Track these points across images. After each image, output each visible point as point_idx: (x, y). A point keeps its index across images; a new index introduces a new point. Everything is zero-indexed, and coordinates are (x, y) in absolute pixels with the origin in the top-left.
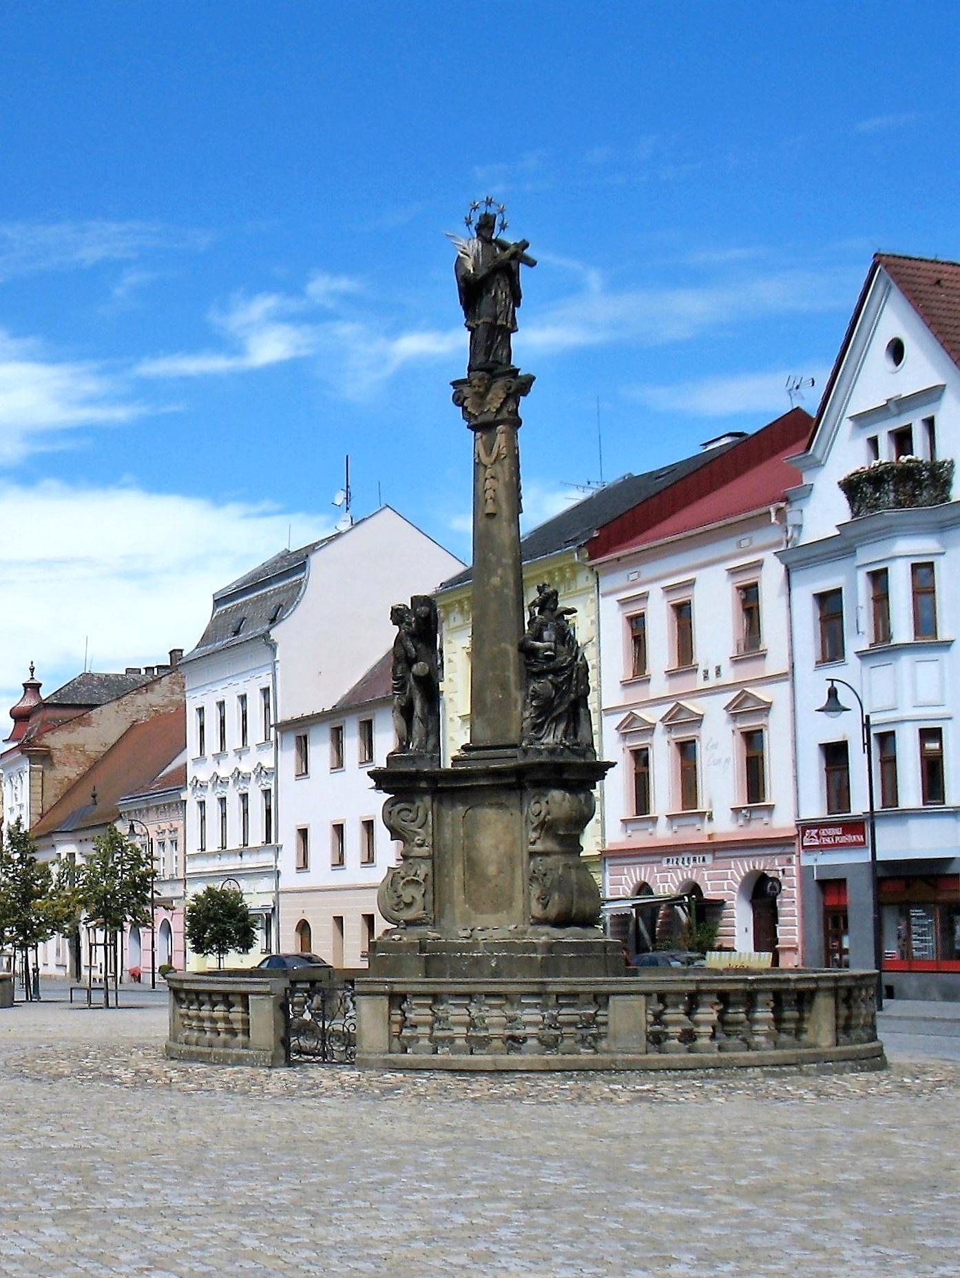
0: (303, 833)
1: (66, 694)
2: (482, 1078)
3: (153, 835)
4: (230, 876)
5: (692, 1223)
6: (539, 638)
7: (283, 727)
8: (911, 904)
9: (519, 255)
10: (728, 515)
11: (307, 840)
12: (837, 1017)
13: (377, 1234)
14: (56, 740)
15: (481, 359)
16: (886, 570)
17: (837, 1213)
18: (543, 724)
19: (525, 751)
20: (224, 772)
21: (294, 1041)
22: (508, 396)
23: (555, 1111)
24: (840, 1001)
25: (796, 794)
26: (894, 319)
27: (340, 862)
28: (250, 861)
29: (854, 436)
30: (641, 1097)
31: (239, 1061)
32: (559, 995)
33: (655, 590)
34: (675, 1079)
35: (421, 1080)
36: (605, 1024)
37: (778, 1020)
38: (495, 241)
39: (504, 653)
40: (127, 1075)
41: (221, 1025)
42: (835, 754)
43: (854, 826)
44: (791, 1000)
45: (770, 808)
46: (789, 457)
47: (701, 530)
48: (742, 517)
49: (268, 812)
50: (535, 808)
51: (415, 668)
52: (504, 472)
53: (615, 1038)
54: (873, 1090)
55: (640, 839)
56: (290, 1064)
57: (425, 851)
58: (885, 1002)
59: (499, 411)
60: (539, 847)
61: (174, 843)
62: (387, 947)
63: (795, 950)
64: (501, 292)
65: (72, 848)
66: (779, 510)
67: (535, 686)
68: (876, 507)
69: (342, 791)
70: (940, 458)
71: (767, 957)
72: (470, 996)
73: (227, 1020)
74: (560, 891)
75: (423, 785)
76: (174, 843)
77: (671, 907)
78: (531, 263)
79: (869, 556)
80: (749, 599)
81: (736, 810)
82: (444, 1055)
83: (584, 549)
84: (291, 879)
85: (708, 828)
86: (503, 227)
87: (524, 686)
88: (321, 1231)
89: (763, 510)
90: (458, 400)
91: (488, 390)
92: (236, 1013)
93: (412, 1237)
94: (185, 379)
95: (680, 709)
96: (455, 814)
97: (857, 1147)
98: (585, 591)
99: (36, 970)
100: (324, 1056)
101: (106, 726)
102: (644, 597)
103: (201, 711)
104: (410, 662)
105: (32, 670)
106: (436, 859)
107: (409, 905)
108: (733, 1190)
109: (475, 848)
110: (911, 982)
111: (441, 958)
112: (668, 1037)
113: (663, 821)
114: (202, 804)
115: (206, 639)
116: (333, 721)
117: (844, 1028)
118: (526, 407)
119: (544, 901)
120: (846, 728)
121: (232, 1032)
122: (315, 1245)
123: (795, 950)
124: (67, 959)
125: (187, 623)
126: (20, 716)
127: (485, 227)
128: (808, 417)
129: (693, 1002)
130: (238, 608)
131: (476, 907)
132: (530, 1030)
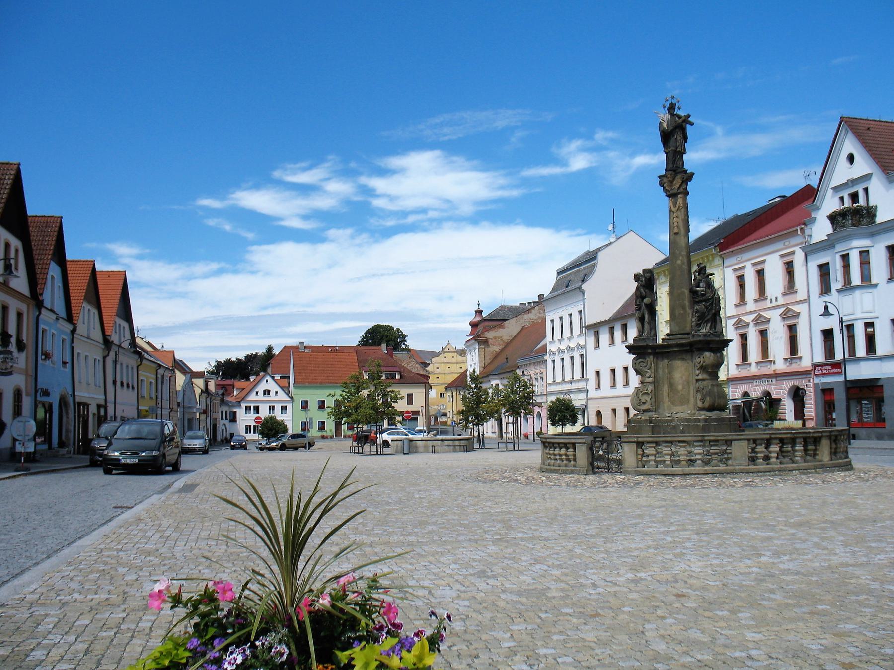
0: (598, 373)
4: (567, 392)
5: (770, 539)
6: (699, 287)
7: (588, 327)
9: (686, 120)
10: (789, 228)
11: (599, 375)
14: (490, 335)
15: (670, 166)
17: (832, 533)
19: (693, 336)
20: (562, 348)
21: (596, 463)
23: (709, 491)
25: (811, 352)
26: (849, 145)
27: (614, 385)
28: (575, 386)
29: (833, 196)
30: (747, 485)
31: (572, 472)
32: (710, 441)
33: (748, 265)
34: (761, 476)
37: (805, 450)
39: (683, 293)
40: (524, 480)
41: (564, 457)
42: (828, 334)
43: (837, 365)
44: (811, 441)
45: (800, 358)
46: (805, 206)
49: (582, 364)
52: (681, 214)
54: (847, 480)
55: (744, 373)
56: (594, 473)
57: (651, 379)
60: (700, 377)
64: (679, 137)
65: (498, 382)
66: (801, 229)
67: (697, 307)
68: (844, 226)
69: (615, 355)
70: (871, 205)
71: (800, 423)
72: (672, 442)
73: (566, 455)
76: (542, 378)
78: (692, 124)
79: (841, 248)
80: (789, 268)
81: (785, 359)
82: (661, 468)
84: (593, 393)
85: (773, 367)
86: (679, 108)
87: (692, 307)
88: (609, 545)
91: (674, 179)
92: (570, 452)
93: (649, 547)
94: (543, 177)
95: (760, 316)
97: (841, 504)
98: (718, 266)
99: (483, 435)
100: (609, 470)
101: (511, 328)
102: (744, 268)
103: (552, 321)
104: (643, 298)
106: (656, 383)
107: (644, 403)
110: (863, 432)
112: (758, 458)
113: (754, 365)
114: (554, 361)
115: (554, 290)
116: (609, 324)
117: (834, 453)
118: (690, 186)
119: (703, 400)
120: (832, 323)
121: (569, 460)
124: (497, 429)
125: (544, 282)
126: (474, 325)
127: (671, 108)
129: (768, 443)
130: (568, 276)
131: (673, 403)
132: (698, 456)
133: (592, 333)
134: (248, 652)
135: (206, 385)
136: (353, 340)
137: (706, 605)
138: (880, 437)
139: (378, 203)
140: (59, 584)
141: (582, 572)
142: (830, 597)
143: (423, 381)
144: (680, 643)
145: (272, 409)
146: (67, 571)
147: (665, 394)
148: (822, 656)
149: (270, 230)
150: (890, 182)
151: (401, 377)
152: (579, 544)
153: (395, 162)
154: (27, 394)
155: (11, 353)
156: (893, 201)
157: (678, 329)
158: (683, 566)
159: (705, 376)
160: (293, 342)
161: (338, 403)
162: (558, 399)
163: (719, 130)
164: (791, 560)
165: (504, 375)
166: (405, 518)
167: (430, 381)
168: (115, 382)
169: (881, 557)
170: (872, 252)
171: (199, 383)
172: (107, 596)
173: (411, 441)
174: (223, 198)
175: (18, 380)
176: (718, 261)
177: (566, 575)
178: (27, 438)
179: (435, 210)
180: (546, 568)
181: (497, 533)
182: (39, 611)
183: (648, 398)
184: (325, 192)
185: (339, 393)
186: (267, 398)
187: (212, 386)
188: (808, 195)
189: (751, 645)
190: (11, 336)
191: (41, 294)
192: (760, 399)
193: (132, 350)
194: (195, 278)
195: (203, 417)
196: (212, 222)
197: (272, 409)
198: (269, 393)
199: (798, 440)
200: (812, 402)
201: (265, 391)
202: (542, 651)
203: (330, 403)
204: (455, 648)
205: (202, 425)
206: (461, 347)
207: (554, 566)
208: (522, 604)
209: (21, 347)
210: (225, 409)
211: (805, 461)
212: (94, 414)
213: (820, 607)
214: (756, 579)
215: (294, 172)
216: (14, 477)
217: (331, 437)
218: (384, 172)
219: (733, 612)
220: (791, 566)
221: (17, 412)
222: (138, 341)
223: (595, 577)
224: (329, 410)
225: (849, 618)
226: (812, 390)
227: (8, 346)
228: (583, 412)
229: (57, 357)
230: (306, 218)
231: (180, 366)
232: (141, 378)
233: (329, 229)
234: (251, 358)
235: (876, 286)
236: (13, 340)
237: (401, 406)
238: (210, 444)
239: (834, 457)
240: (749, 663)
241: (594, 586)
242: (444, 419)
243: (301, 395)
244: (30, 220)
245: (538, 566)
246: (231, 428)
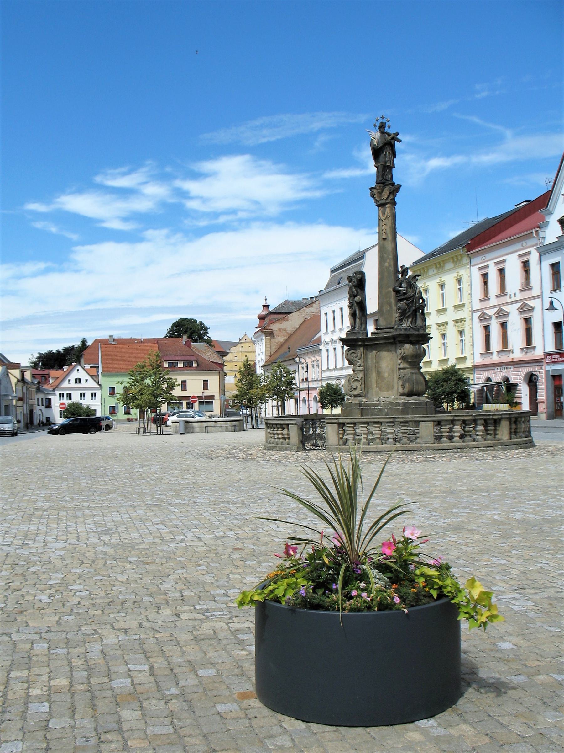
1: (279, 309)
6: (401, 287)
10: (526, 231)
12: (511, 429)
14: (275, 327)
15: (380, 178)
18: (403, 319)
19: (396, 330)
22: (390, 193)
24: (512, 422)
30: (427, 460)
31: (286, 449)
33: (491, 263)
34: (445, 453)
36: (418, 433)
38: (386, 133)
47: (507, 240)
48: (522, 234)
52: (389, 222)
53: (422, 438)
55: (487, 360)
57: (361, 368)
59: (387, 199)
60: (401, 366)
61: (318, 365)
63: (543, 402)
64: (388, 152)
67: (399, 304)
72: (367, 423)
73: (283, 434)
74: (409, 382)
75: (360, 343)
76: (318, 365)
80: (526, 265)
81: (522, 349)
83: (465, 248)
86: (389, 127)
89: (530, 231)
90: (372, 195)
91: (382, 191)
92: (285, 432)
94: (344, 179)
96: (372, 354)
98: (465, 265)
101: (294, 321)
103: (326, 314)
105: (266, 300)
106: (365, 371)
107: (355, 389)
109: (380, 367)
111: (367, 409)
113: (495, 354)
114: (327, 350)
115: (328, 286)
117: (514, 432)
119: (403, 386)
121: (284, 438)
123: (543, 402)
126: (261, 318)
127: (382, 127)
129: (453, 422)
130: (340, 274)
131: (380, 389)
132: (390, 436)
135: (23, 375)
136: (161, 332)
139: (192, 205)
145: (83, 395)
149: (93, 231)
151: (198, 365)
153: (208, 166)
160: (104, 335)
161: (126, 389)
162: (328, 385)
163: (509, 133)
167: (226, 369)
171: (16, 373)
173: (187, 422)
174: (48, 202)
179: (242, 210)
184: (143, 195)
185: (126, 381)
186: (78, 386)
187: (28, 376)
194: (25, 277)
195: (20, 403)
196: (39, 225)
197: (83, 395)
198: (80, 382)
199: (479, 422)
200: (544, 387)
201: (76, 380)
203: (120, 390)
210: (41, 396)
215: (114, 177)
217: (136, 420)
218: (196, 176)
224: (118, 396)
226: (543, 376)
230: (125, 219)
233: (147, 229)
234: (68, 350)
237: (177, 392)
239: (513, 436)
246: (46, 413)
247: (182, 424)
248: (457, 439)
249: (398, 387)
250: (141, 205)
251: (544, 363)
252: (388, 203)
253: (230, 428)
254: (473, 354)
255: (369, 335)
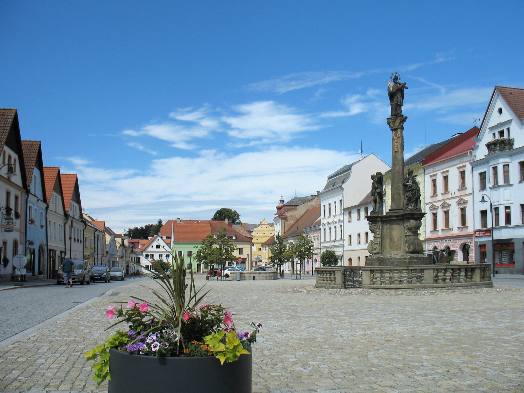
0: (350, 236)
2: (393, 290)
3: (312, 237)
4: (332, 247)
5: (441, 317)
6: (408, 182)
7: (345, 210)
8: (502, 250)
9: (404, 86)
10: (463, 152)
11: (350, 236)
13: (365, 320)
14: (288, 214)
15: (394, 112)
16: (497, 167)
17: (477, 315)
19: (404, 210)
20: (330, 221)
21: (347, 283)
23: (410, 297)
25: (474, 223)
26: (499, 103)
27: (359, 243)
28: (337, 243)
29: (489, 133)
30: (432, 294)
31: (333, 287)
32: (412, 270)
33: (439, 173)
35: (378, 291)
39: (400, 186)
40: (305, 291)
41: (328, 279)
42: (484, 213)
43: (488, 231)
44: (469, 270)
45: (467, 227)
46: (473, 138)
49: (341, 231)
50: (407, 224)
51: (377, 190)
52: (399, 141)
54: (489, 292)
55: (435, 236)
56: (345, 288)
57: (379, 236)
58: (495, 275)
60: (408, 234)
61: (318, 239)
62: (369, 260)
64: (399, 96)
65: (292, 241)
66: (470, 152)
67: (407, 194)
68: (495, 151)
69: (361, 225)
70: (511, 138)
71: (465, 262)
73: (330, 278)
75: (379, 219)
76: (318, 239)
77: (442, 252)
79: (493, 163)
80: (463, 173)
81: (459, 228)
82: (383, 285)
84: (347, 247)
85: (451, 232)
86: (400, 79)
87: (404, 194)
88: (351, 320)
90: (388, 123)
91: (396, 120)
92: (332, 276)
93: (373, 321)
97: (484, 303)
98: (422, 173)
99: (283, 271)
100: (354, 286)
101: (301, 210)
102: (436, 175)
103: (324, 206)
104: (376, 189)
106: (382, 238)
107: (375, 249)
108: (452, 311)
110: (502, 270)
112: (439, 279)
113: (440, 231)
114: (325, 229)
115: (326, 188)
116: (358, 208)
117: (483, 277)
118: (405, 124)
120: (486, 206)
121: (331, 281)
122: (350, 323)
124: (291, 269)
125: (321, 184)
126: (279, 208)
127: (395, 79)
128: (478, 128)
129: (445, 270)
133: (347, 213)
134: (159, 335)
135: (123, 242)
136: (209, 217)
137: (402, 345)
138: (512, 273)
140: (48, 333)
141: (335, 331)
142: (470, 342)
143: (249, 241)
144: (386, 360)
145: (161, 256)
146: (51, 328)
147: (387, 244)
148: (462, 365)
149: (166, 150)
150: (522, 125)
151: (236, 238)
152: (335, 319)
153: (245, 108)
154: (21, 244)
155: (12, 219)
156: (523, 136)
157: (396, 207)
158: (391, 328)
159: (410, 234)
160: (174, 218)
161: (199, 252)
163: (443, 90)
164: (452, 326)
165: (296, 238)
166: (238, 308)
167: (253, 241)
168: (70, 238)
169: (502, 325)
170: (511, 165)
172: (74, 338)
173: (242, 273)
174: (139, 130)
175: (15, 235)
176: (421, 171)
177: (326, 332)
178: (22, 267)
179: (265, 138)
180: (315, 329)
181: (289, 314)
182: (38, 345)
183: (377, 248)
184: (200, 126)
186: (158, 250)
187: (126, 243)
188: (475, 132)
189: (424, 361)
190: (11, 210)
191: (29, 186)
192: (444, 251)
193: (81, 220)
194: (121, 179)
195: (121, 260)
196: (131, 144)
197: (161, 256)
198: (159, 247)
199: (462, 270)
200: (473, 252)
201: (157, 246)
202: (311, 363)
204: (264, 361)
205: (121, 264)
206: (271, 221)
207: (320, 329)
208: (302, 344)
209: (17, 216)
210: (133, 256)
211: (466, 282)
212: (59, 256)
213: (464, 346)
214: (431, 334)
215: (182, 114)
216: (15, 288)
218: (237, 114)
219: (416, 347)
220: (451, 329)
221: (15, 253)
222: (84, 216)
223: (342, 333)
225: (479, 350)
226: (473, 245)
227: (10, 215)
228: (341, 259)
229: (38, 223)
230: (188, 142)
231: (107, 230)
232: (85, 236)
233: (202, 149)
234: (148, 227)
235: (512, 185)
236: (13, 212)
238: (125, 276)
240: (422, 368)
241: (342, 337)
242: (260, 263)
243: (178, 248)
244: (22, 142)
245: (311, 329)
247: (239, 274)
248: (448, 280)
249: (404, 247)
250: (199, 133)
251: (474, 237)
252: (399, 128)
253: (268, 277)
254: (425, 232)
255: (384, 214)
